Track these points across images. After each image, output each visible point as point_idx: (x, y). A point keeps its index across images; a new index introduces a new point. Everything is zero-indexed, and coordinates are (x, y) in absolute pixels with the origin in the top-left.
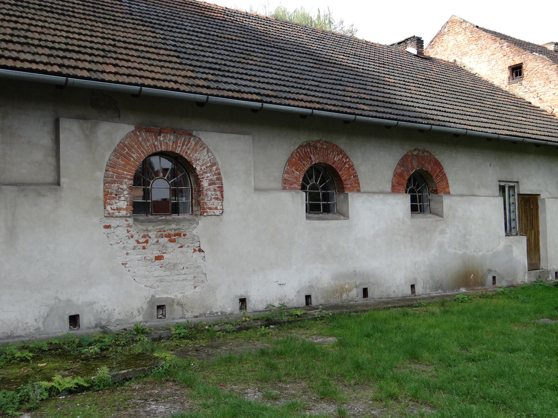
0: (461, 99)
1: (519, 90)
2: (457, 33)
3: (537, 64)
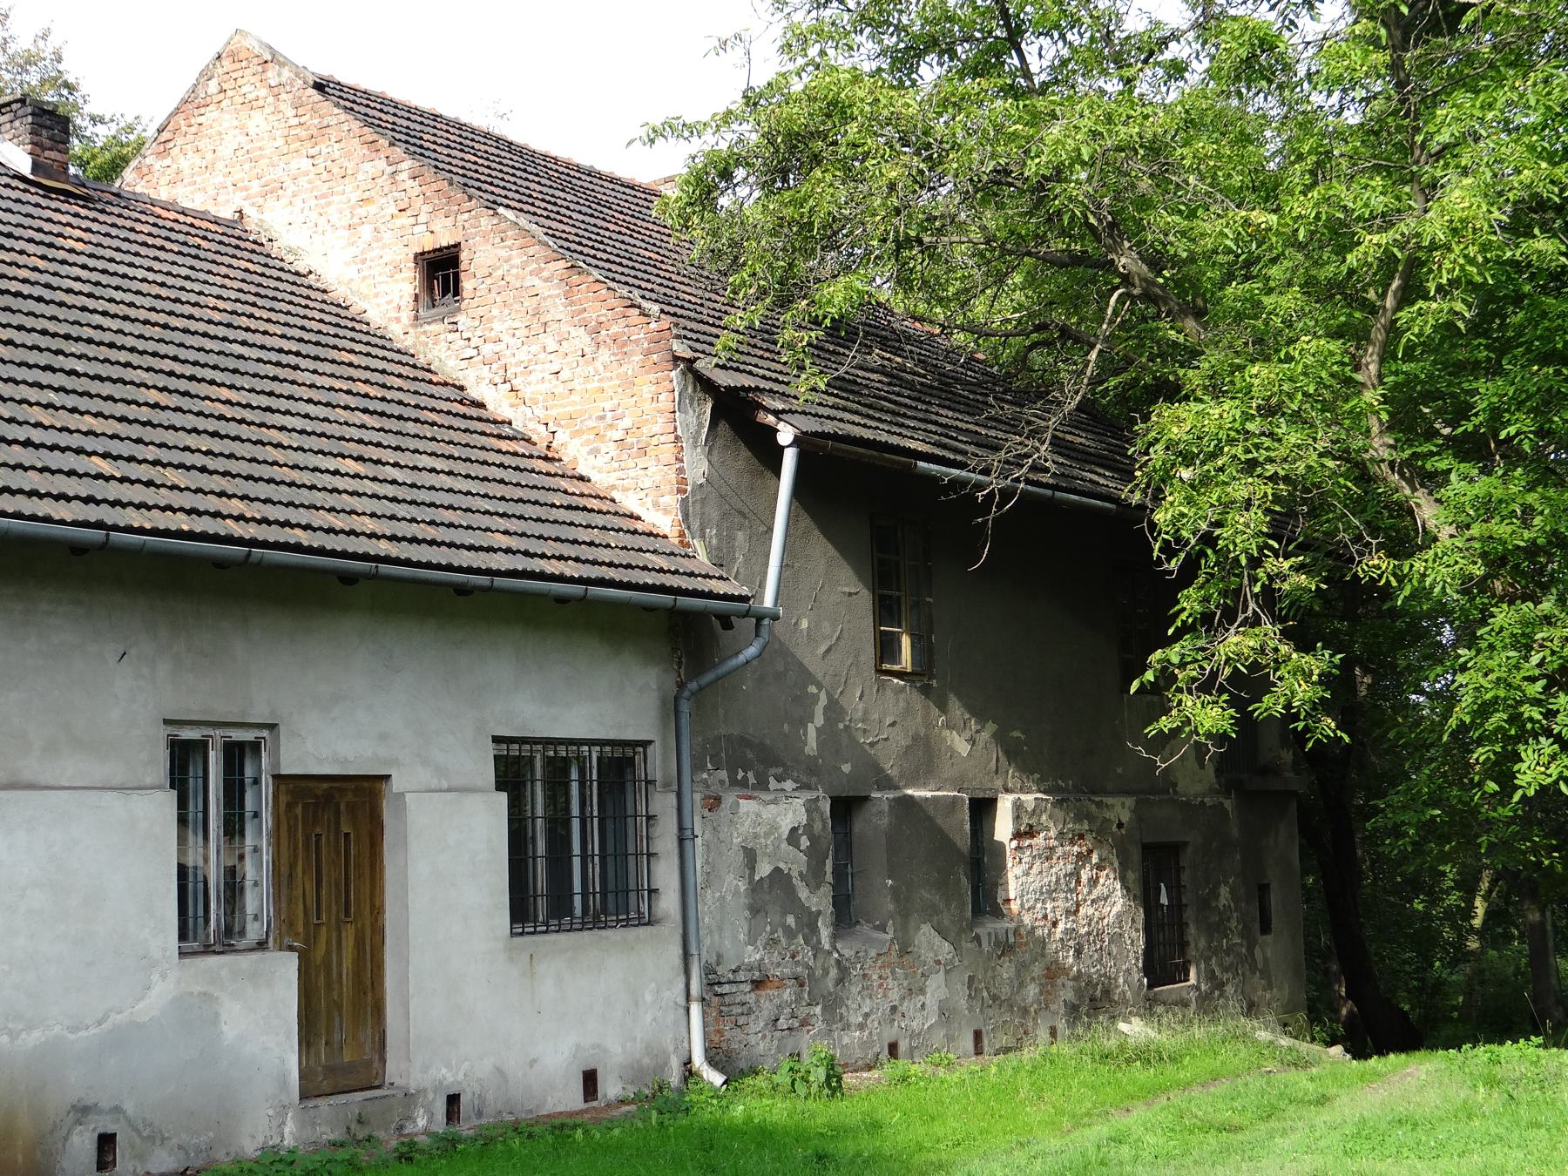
0: (72, 373)
1: (442, 349)
2: (250, 105)
3: (503, 253)
